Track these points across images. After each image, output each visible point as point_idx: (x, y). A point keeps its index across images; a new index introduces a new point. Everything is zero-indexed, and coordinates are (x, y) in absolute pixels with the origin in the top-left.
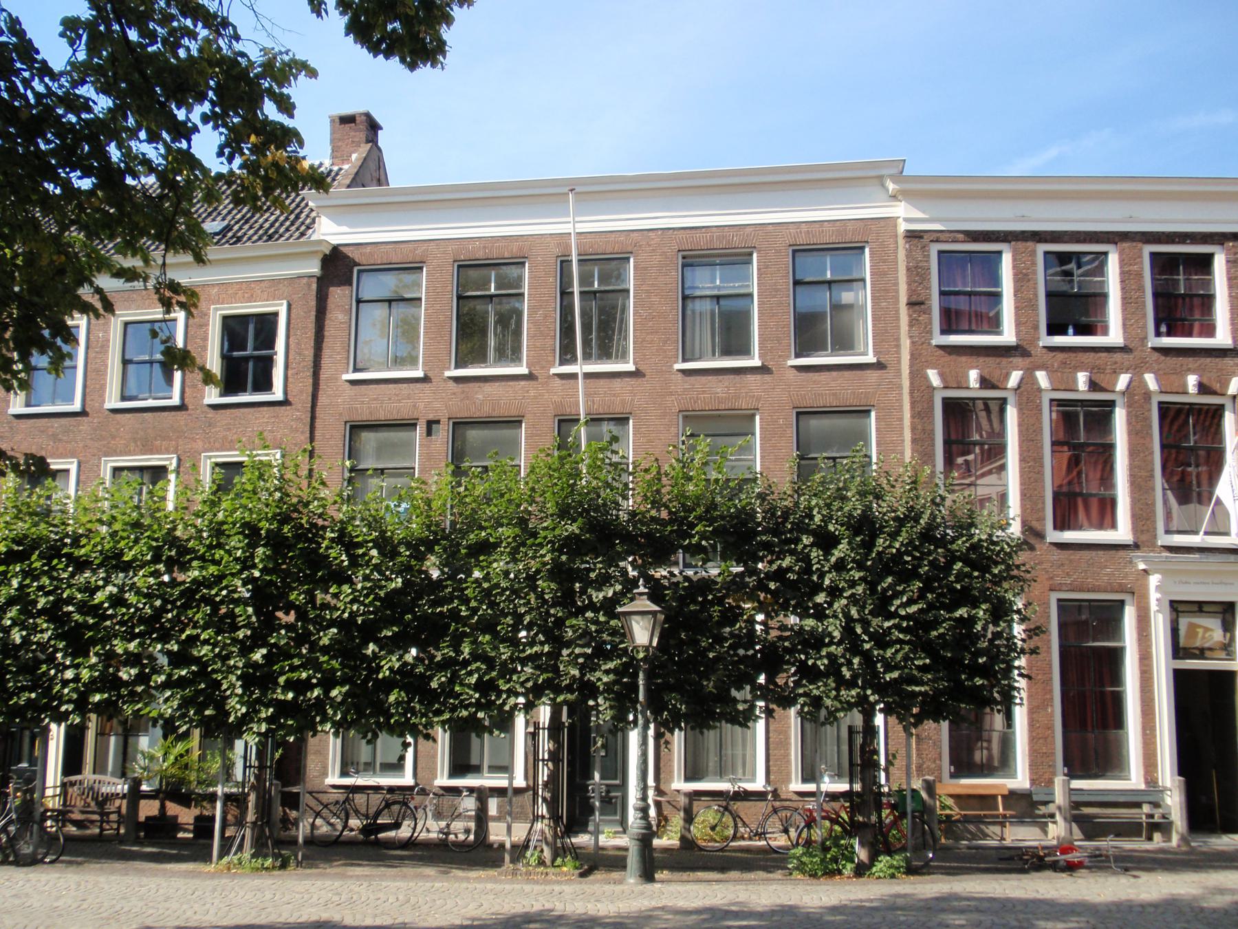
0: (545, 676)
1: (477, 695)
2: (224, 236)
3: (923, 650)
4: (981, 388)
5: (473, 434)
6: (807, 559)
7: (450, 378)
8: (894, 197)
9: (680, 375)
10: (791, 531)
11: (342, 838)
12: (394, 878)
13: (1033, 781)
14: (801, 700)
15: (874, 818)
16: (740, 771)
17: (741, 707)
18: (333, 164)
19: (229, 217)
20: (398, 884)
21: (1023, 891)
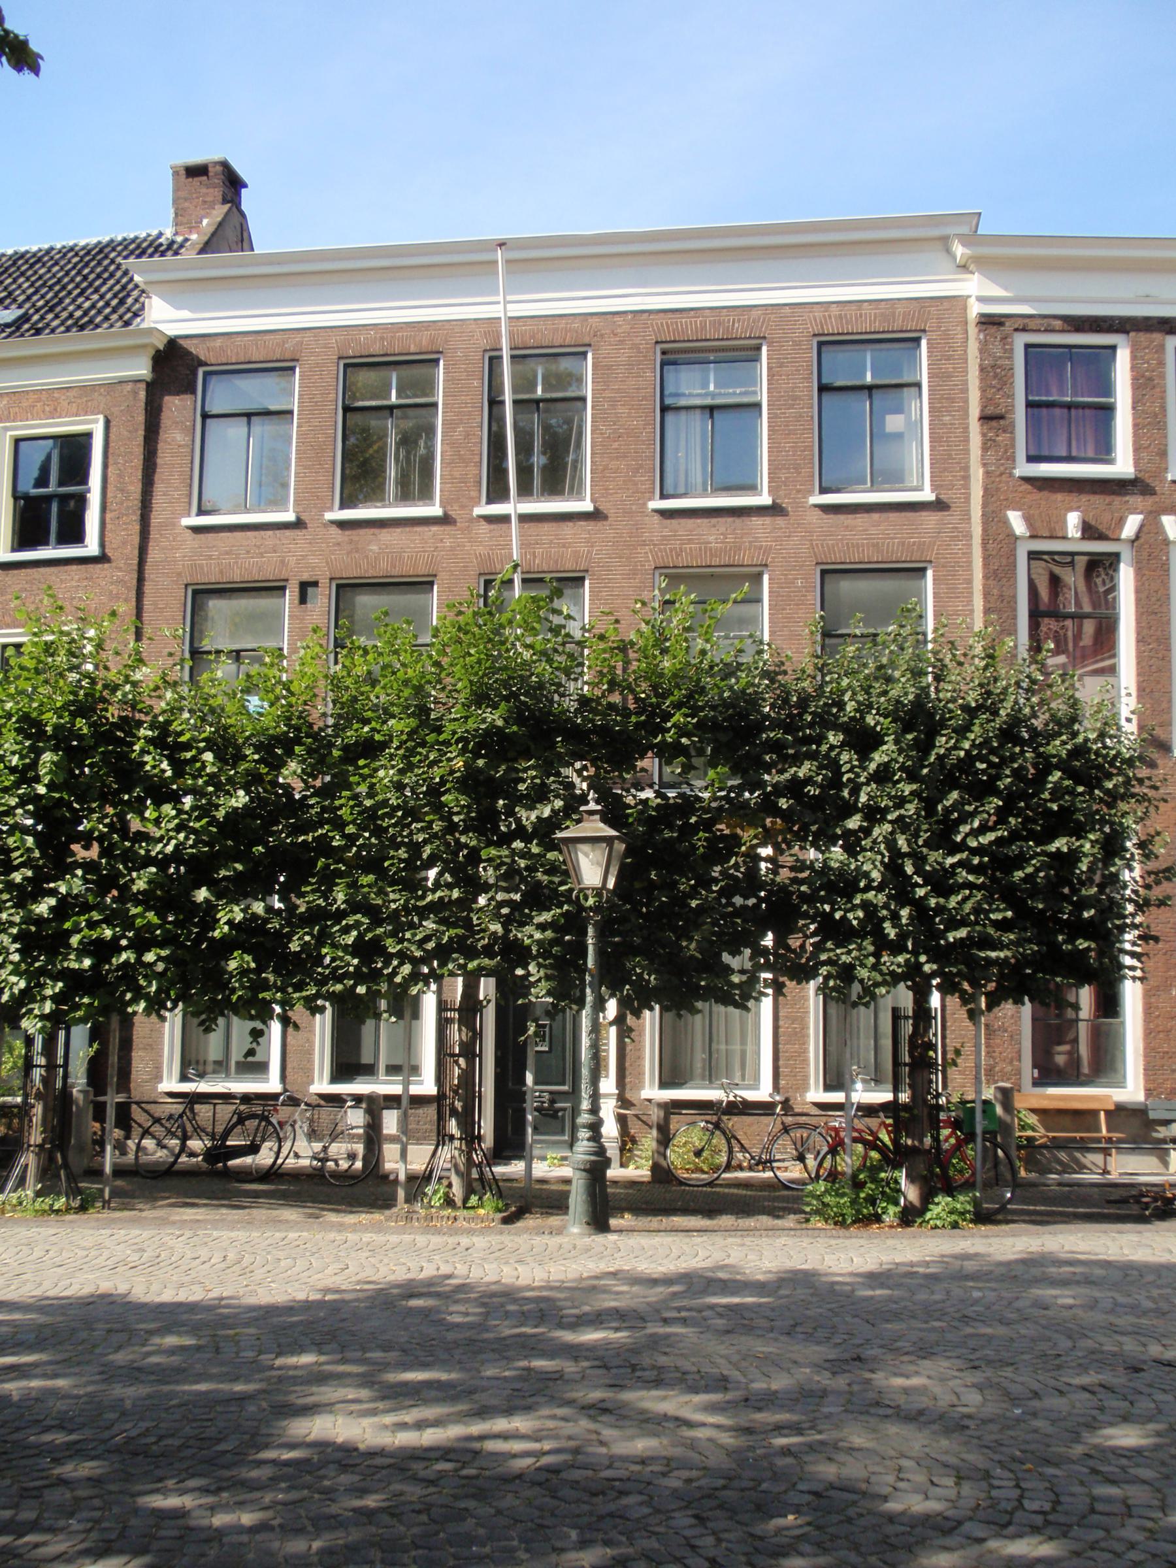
0: (453, 932)
1: (356, 961)
2: (18, 328)
3: (1003, 899)
4: (1083, 538)
5: (366, 602)
6: (834, 766)
7: (333, 522)
8: (964, 267)
9: (657, 517)
10: (811, 725)
11: (176, 1167)
12: (232, 1226)
13: (1149, 1092)
14: (824, 970)
15: (928, 1141)
16: (738, 1074)
17: (736, 979)
18: (176, 234)
19: (27, 305)
20: (233, 1234)
21: (1149, 1251)
